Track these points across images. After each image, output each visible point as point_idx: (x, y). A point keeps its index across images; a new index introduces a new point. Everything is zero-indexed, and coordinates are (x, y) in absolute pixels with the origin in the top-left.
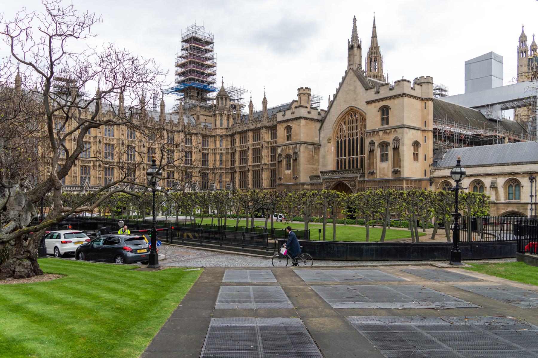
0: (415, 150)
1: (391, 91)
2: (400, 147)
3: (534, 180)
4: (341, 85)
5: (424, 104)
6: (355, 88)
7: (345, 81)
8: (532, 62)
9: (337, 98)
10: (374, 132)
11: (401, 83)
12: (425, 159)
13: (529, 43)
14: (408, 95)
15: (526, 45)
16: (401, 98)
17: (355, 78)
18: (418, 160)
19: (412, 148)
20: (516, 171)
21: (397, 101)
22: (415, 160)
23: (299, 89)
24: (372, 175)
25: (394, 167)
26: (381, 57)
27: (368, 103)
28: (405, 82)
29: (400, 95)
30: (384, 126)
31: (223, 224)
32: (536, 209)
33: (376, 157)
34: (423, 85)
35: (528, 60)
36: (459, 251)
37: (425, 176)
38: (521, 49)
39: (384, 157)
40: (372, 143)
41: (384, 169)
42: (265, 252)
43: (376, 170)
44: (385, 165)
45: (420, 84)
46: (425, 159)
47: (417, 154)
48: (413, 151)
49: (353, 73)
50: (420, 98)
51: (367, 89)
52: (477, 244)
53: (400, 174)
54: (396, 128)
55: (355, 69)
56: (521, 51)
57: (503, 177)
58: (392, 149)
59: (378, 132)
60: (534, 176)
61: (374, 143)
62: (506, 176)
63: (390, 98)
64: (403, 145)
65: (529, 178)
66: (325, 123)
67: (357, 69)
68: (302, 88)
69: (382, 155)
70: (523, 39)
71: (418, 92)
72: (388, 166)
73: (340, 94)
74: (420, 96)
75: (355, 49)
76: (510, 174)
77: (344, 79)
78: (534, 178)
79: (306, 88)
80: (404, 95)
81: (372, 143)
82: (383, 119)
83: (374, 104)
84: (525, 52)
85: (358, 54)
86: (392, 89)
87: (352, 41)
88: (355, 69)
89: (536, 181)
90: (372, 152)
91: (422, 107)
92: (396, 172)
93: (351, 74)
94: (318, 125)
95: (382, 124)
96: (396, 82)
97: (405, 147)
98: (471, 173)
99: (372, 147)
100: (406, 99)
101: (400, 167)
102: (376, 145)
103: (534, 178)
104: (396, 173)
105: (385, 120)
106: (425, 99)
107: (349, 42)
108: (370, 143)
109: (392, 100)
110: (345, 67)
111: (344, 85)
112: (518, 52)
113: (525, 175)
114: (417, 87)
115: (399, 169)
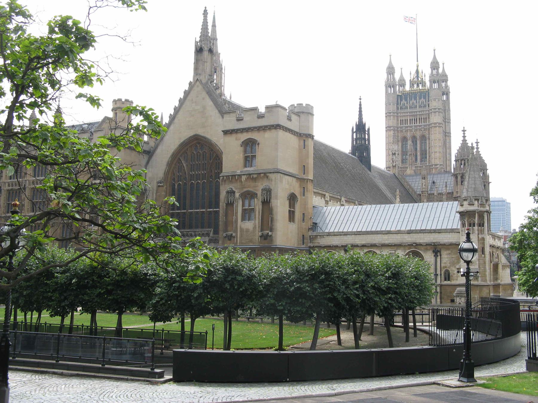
0: (290, 207)
1: (260, 120)
2: (272, 201)
3: (439, 254)
4: (182, 102)
5: (302, 142)
6: (204, 108)
7: (189, 98)
8: (401, 100)
9: (176, 120)
10: (233, 178)
11: (274, 109)
12: (304, 220)
13: (397, 76)
14: (283, 127)
15: (394, 78)
16: (273, 131)
17: (204, 94)
18: (294, 221)
19: (287, 203)
20: (418, 241)
21: (268, 134)
22: (290, 221)
23: (115, 101)
24: (230, 240)
25: (262, 230)
26: (222, 69)
27: (226, 132)
28: (280, 109)
29: (273, 126)
30: (246, 169)
31: (34, 321)
32: (441, 293)
33: (237, 213)
34: (302, 115)
35: (396, 97)
36: (472, 361)
37: (303, 243)
38: (389, 82)
39: (247, 214)
40: (231, 193)
41: (247, 230)
42: (99, 368)
43: (236, 232)
44: (248, 225)
45: (298, 114)
46: (304, 220)
47: (293, 212)
48: (287, 209)
49: (200, 87)
50: (297, 133)
51: (222, 113)
52: (455, 348)
53: (272, 241)
54: (265, 175)
55: (204, 81)
56: (390, 85)
57: (402, 248)
58: (260, 203)
59: (240, 176)
60: (438, 248)
61: (234, 192)
62: (407, 248)
63: (259, 129)
64: (277, 199)
65: (434, 252)
66: (154, 158)
67: (207, 83)
68: (120, 100)
69: (244, 211)
70: (391, 70)
71: (294, 125)
72: (255, 227)
73: (179, 116)
74: (297, 130)
75: (206, 53)
76: (410, 245)
77: (187, 93)
78: (438, 251)
79: (127, 101)
80: (277, 127)
81: (231, 193)
82: (246, 158)
83: (234, 136)
84: (393, 87)
85: (209, 60)
86: (261, 116)
87: (200, 41)
88: (204, 81)
89: (440, 255)
90: (230, 205)
91: (299, 146)
92: (265, 237)
93: (199, 88)
94: (146, 157)
95: (245, 166)
96: (267, 108)
97: (279, 201)
98: (363, 242)
99: (231, 199)
100: (281, 133)
101: (271, 230)
102: (237, 195)
103: (438, 251)
104: (265, 239)
105: (249, 160)
106: (304, 134)
107: (196, 42)
108: (228, 192)
109: (262, 133)
110: (190, 77)
111: (187, 103)
112: (386, 87)
113: (428, 247)
114: (294, 117)
115: (270, 233)
